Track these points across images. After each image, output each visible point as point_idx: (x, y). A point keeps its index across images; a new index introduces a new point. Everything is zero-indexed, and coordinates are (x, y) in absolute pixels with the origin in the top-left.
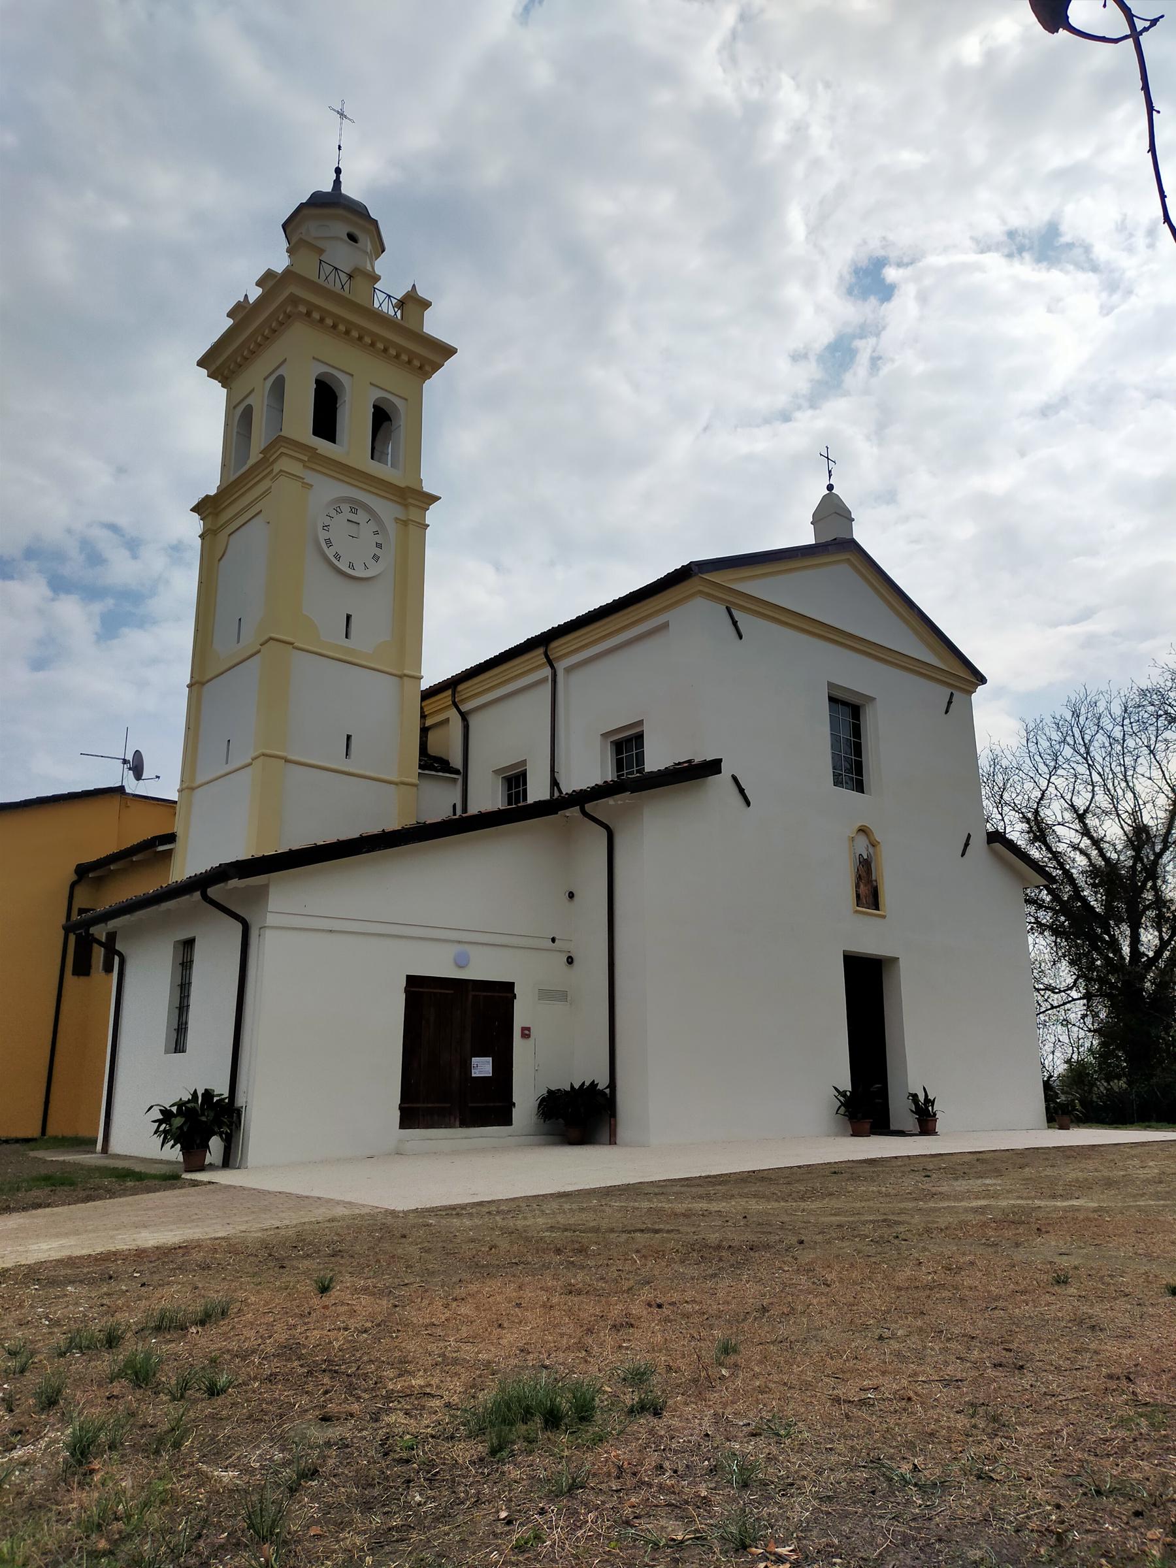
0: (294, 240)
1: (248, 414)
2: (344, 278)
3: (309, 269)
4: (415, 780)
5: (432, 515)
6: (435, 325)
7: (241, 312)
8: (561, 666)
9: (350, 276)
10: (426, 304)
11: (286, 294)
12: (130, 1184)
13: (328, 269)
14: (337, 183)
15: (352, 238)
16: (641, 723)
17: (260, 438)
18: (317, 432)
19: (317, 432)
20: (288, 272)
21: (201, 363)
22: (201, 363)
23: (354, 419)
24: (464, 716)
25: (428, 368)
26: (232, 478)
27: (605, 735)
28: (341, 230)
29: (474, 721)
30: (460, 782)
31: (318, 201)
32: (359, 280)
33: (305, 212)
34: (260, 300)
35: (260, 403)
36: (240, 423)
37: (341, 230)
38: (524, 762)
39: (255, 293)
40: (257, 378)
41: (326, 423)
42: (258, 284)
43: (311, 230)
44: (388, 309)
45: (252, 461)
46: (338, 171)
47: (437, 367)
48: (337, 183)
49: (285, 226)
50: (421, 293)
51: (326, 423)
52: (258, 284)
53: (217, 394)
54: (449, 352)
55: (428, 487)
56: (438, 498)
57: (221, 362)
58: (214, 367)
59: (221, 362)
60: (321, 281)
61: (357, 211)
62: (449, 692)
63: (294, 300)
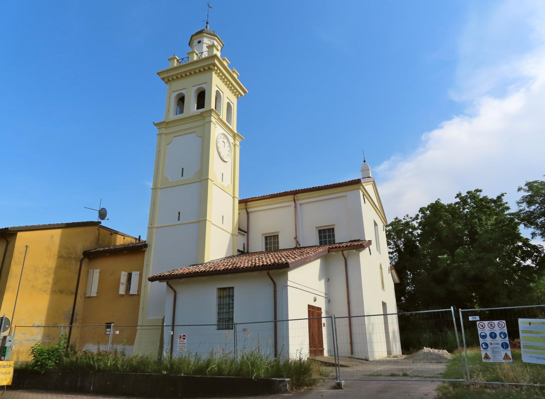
4: (237, 234)
8: (298, 202)
16: (334, 225)
24: (248, 213)
27: (317, 228)
29: (251, 215)
30: (246, 236)
38: (278, 232)
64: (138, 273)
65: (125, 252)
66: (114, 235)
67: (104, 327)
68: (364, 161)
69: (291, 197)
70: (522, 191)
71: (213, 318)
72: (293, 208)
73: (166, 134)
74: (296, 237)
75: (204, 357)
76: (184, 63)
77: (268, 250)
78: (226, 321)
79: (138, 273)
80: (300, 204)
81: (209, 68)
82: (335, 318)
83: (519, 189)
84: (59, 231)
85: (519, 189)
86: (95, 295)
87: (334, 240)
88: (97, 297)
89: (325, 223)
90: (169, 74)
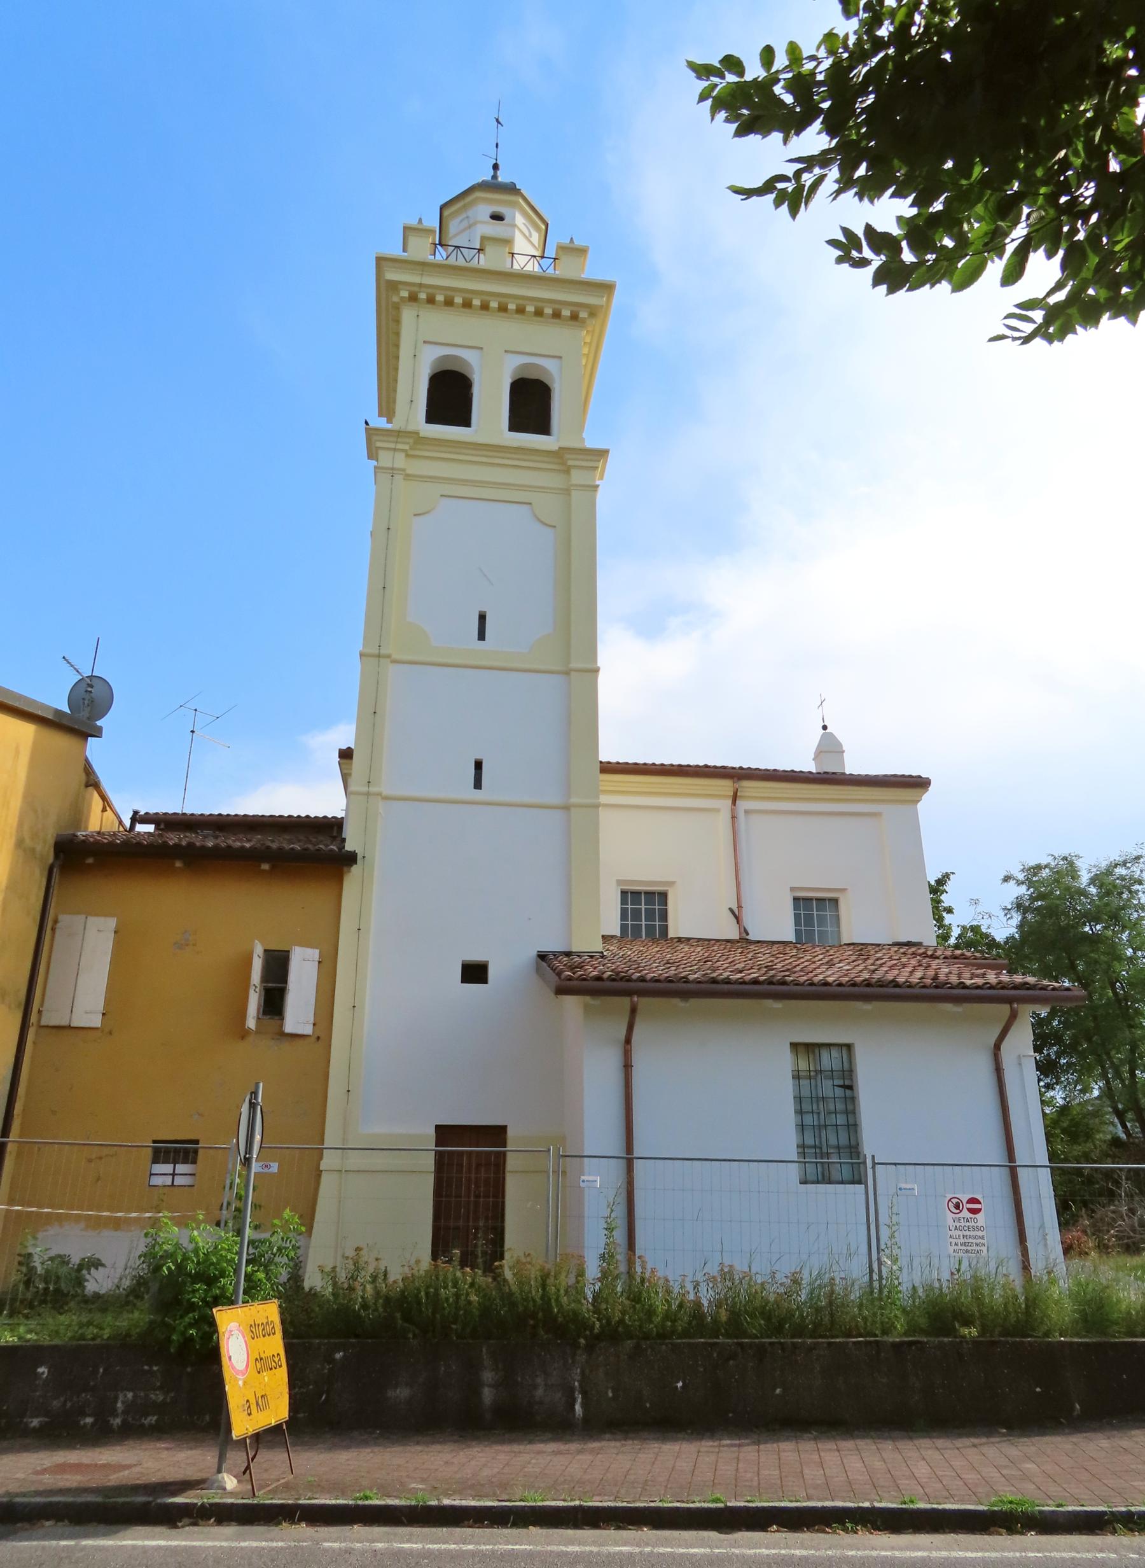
8: (742, 805)
62: (1005, 1009)
64: (314, 954)
65: (265, 866)
66: (91, 789)
67: (149, 1153)
68: (825, 727)
69: (726, 786)
70: (1012, 882)
71: (784, 1138)
72: (724, 816)
73: (408, 477)
74: (740, 907)
75: (785, 1270)
76: (461, 262)
77: (630, 932)
78: (832, 1146)
79: (314, 954)
80: (747, 812)
81: (574, 317)
82: (874, 1164)
83: (1007, 879)
84: (27, 731)
85: (1007, 879)
86: (96, 1021)
87: (664, 930)
88: (106, 1031)
89: (815, 881)
90: (428, 280)
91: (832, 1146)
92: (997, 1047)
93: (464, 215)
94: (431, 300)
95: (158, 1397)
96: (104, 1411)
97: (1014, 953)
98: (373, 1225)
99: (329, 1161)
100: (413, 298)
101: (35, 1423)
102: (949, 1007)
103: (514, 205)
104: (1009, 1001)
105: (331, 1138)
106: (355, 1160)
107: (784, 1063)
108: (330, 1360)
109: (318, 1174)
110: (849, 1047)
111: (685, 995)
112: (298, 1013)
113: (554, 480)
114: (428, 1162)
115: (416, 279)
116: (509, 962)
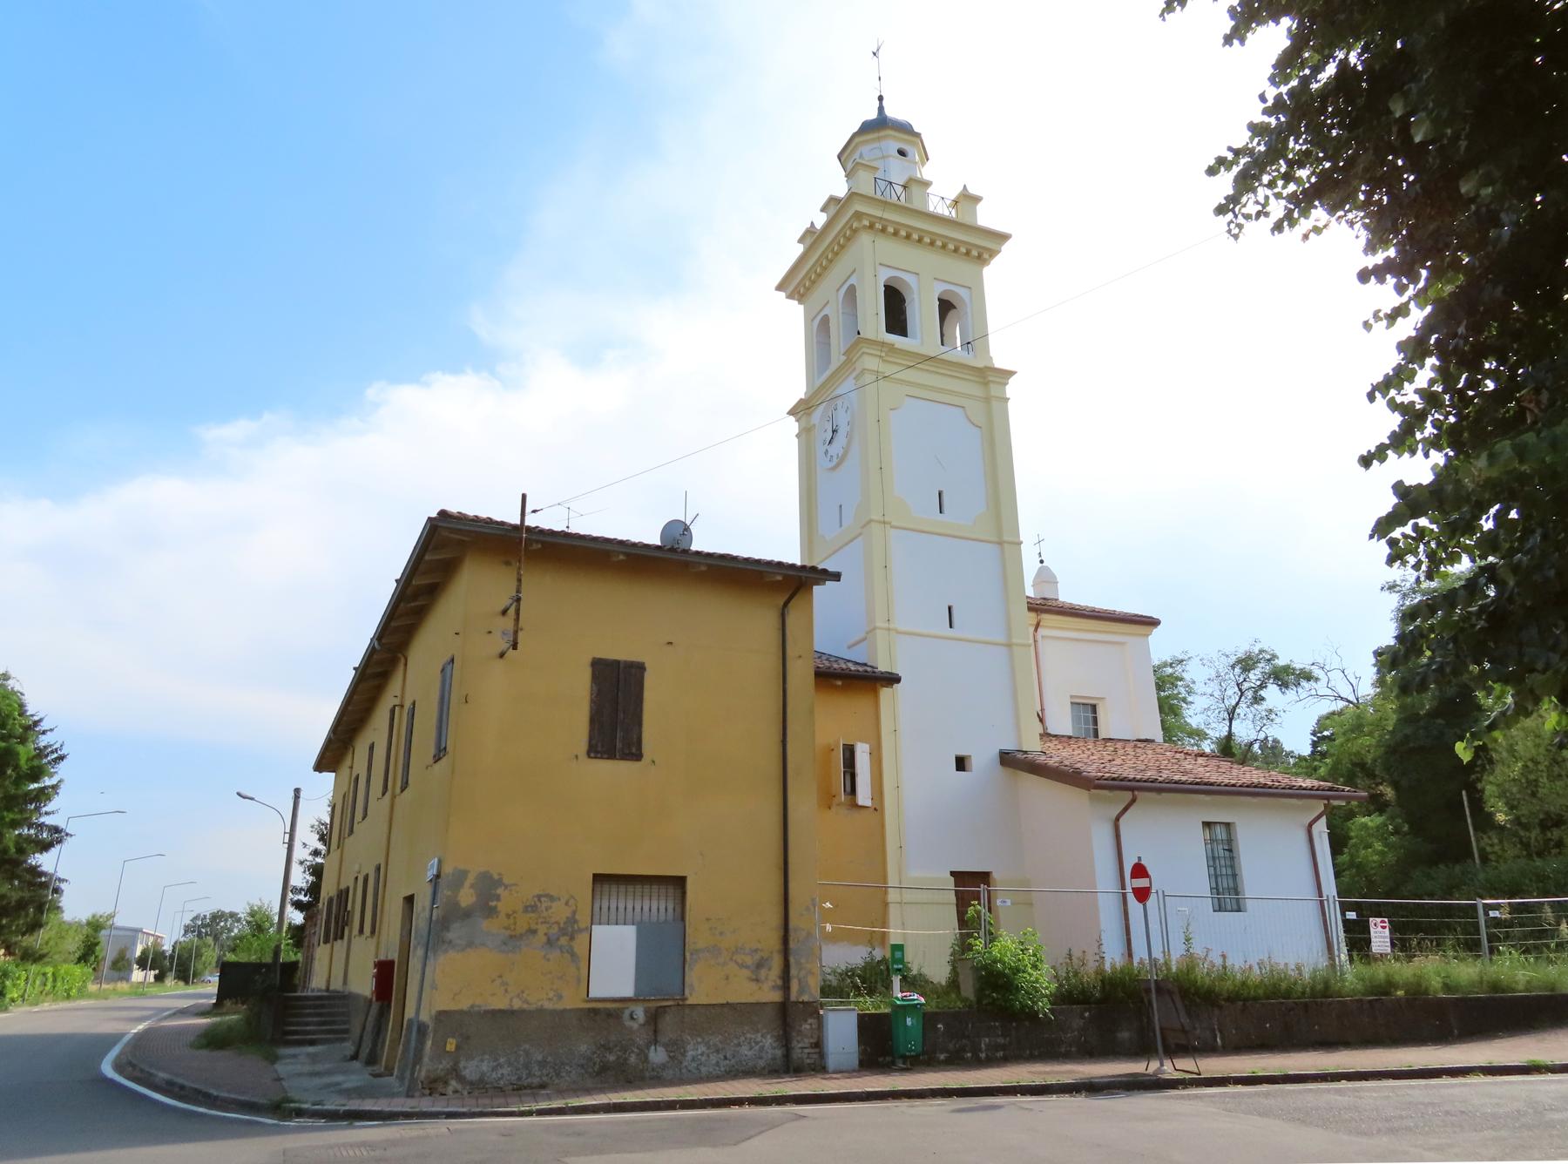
0: (850, 166)
1: (825, 321)
2: (899, 190)
3: (865, 185)
5: (1012, 389)
6: (986, 217)
7: (811, 237)
9: (905, 187)
10: (977, 199)
11: (850, 213)
12: (839, 683)
13: (882, 184)
14: (881, 109)
15: (902, 153)
17: (838, 343)
18: (890, 329)
19: (890, 329)
20: (852, 195)
21: (779, 288)
22: (779, 288)
23: (922, 312)
25: (986, 256)
26: (818, 383)
28: (893, 146)
31: (867, 127)
32: (914, 189)
33: (857, 140)
34: (828, 225)
35: (835, 312)
36: (819, 331)
37: (893, 146)
39: (820, 220)
40: (829, 290)
41: (896, 319)
42: (800, 241)
43: (867, 152)
44: (943, 210)
45: (833, 367)
46: (881, 98)
47: (993, 253)
48: (881, 109)
49: (839, 157)
50: (972, 190)
51: (896, 319)
52: (800, 241)
53: (795, 312)
54: (1003, 237)
55: (999, 363)
56: (1012, 373)
57: (797, 284)
58: (791, 288)
59: (797, 284)
60: (878, 196)
61: (905, 129)
62: (1128, 795)
63: (858, 215)
78: (1227, 891)
90: (887, 216)
91: (1227, 891)
92: (1117, 819)
93: (876, 145)
94: (883, 230)
95: (1001, 1040)
96: (976, 1050)
97: (1306, 766)
98: (926, 939)
99: (893, 896)
100: (871, 226)
101: (942, 1057)
102: (1294, 801)
103: (913, 144)
104: (1132, 789)
105: (892, 880)
106: (909, 896)
107: (1199, 834)
108: (1082, 1017)
109: (886, 904)
110: (1228, 825)
111: (1160, 790)
112: (864, 796)
113: (977, 390)
114: (953, 898)
115: (878, 213)
116: (983, 758)
